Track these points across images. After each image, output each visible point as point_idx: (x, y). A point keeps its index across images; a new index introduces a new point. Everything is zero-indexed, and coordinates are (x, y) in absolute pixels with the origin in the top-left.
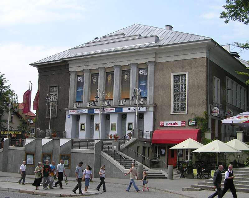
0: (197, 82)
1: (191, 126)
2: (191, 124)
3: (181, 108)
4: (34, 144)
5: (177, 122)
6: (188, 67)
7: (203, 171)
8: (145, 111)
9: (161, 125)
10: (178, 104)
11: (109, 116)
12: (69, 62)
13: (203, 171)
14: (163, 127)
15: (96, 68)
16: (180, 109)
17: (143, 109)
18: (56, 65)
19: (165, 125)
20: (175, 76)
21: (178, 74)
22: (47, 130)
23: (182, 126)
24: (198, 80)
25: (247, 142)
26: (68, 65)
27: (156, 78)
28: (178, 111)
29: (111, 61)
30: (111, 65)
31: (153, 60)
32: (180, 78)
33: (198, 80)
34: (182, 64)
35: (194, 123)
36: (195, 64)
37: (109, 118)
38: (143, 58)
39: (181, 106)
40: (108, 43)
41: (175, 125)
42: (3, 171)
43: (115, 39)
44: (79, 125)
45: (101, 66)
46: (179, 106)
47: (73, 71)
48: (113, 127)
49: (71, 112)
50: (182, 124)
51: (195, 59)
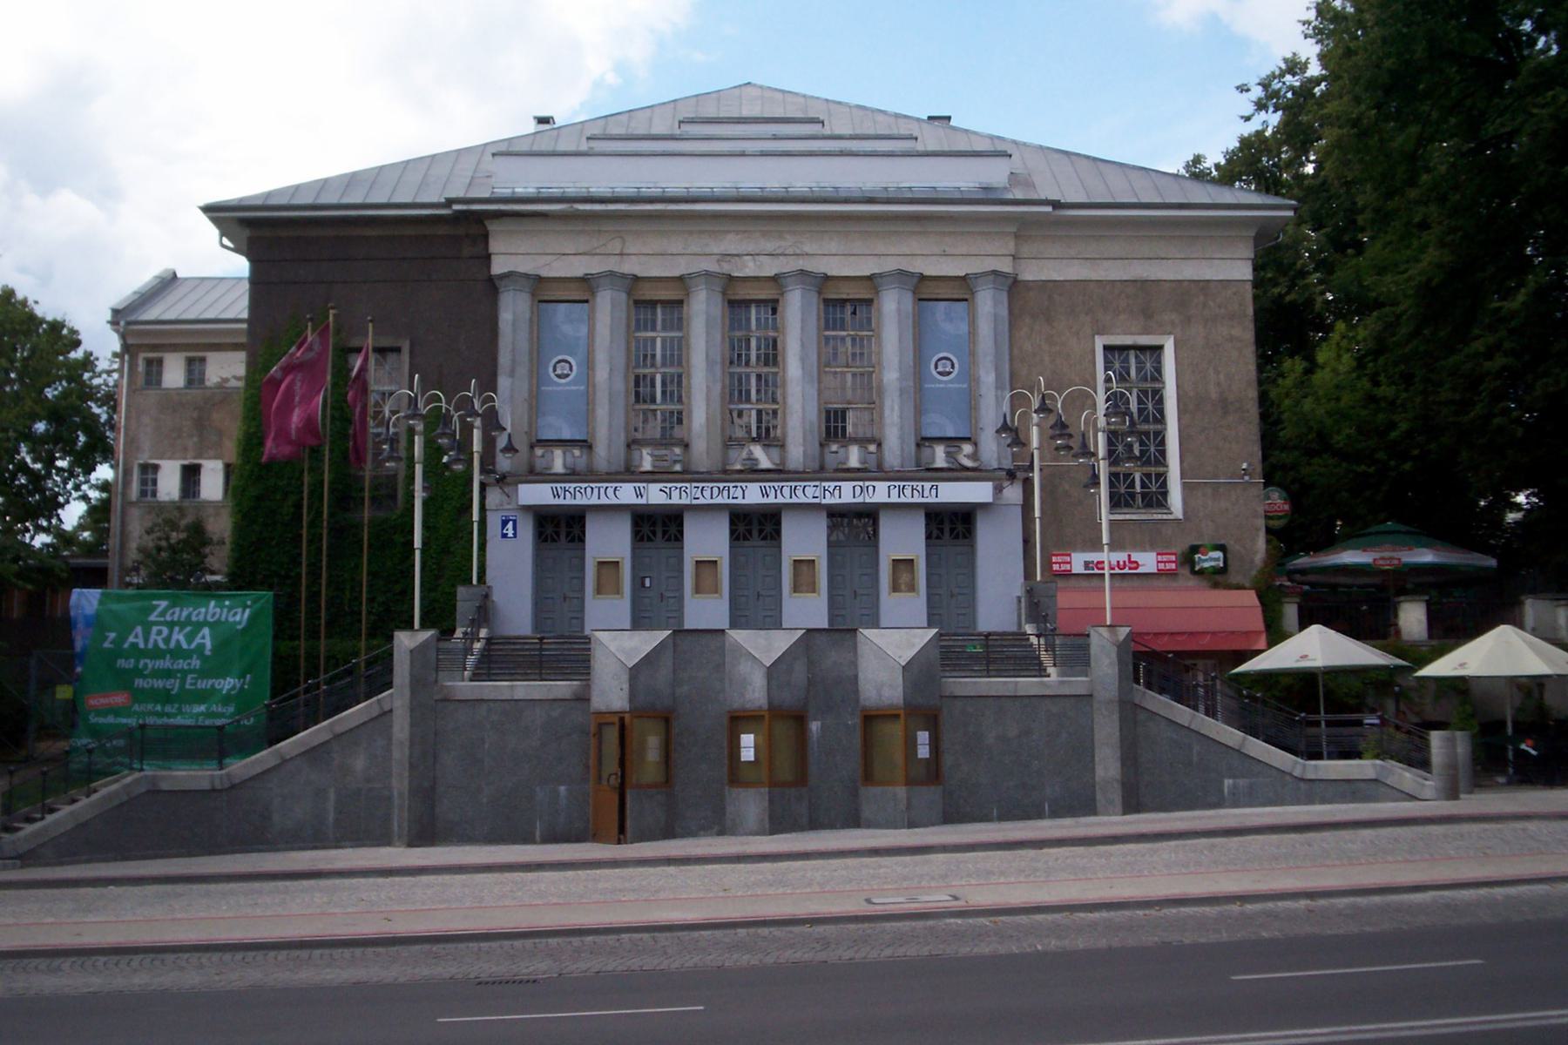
0: (1219, 384)
1: (1201, 572)
2: (1206, 565)
3: (1144, 495)
4: (667, 660)
5: (1135, 556)
6: (1174, 316)
7: (562, 788)
8: (989, 499)
9: (1056, 567)
10: (1127, 476)
11: (779, 523)
12: (492, 227)
13: (1523, 746)
14: (1068, 575)
15: (677, 274)
16: (1139, 499)
17: (975, 492)
18: (410, 231)
19: (1078, 568)
20: (1107, 348)
21: (1128, 340)
22: (462, 591)
23: (1160, 574)
24: (1222, 376)
25: (1380, 642)
26: (485, 237)
27: (1016, 351)
28: (1128, 505)
29: (770, 246)
30: (769, 268)
31: (1005, 266)
32: (1133, 360)
33: (1222, 376)
34: (1145, 299)
35: (1217, 559)
36: (1205, 305)
37: (778, 532)
38: (949, 250)
39: (1143, 485)
40: (743, 154)
41: (1126, 571)
42: (410, 845)
43: (775, 138)
44: (681, 571)
45: (712, 267)
46: (1132, 485)
47: (526, 276)
48: (904, 578)
49: (537, 494)
50: (1161, 566)
51: (1204, 286)
